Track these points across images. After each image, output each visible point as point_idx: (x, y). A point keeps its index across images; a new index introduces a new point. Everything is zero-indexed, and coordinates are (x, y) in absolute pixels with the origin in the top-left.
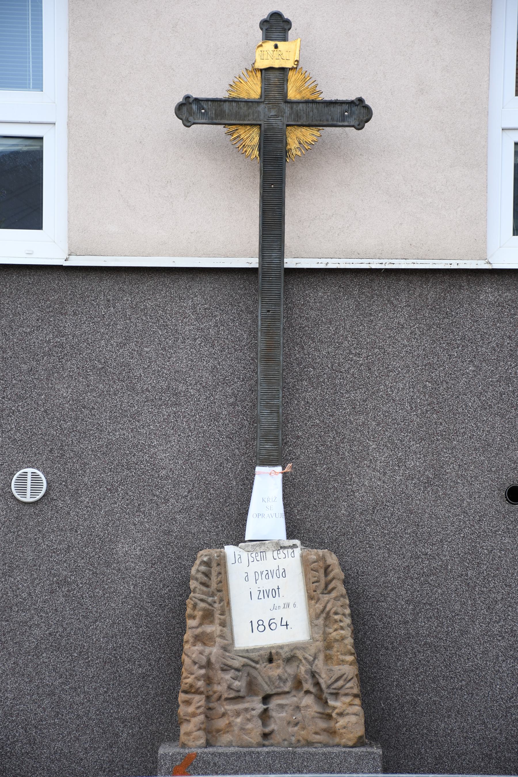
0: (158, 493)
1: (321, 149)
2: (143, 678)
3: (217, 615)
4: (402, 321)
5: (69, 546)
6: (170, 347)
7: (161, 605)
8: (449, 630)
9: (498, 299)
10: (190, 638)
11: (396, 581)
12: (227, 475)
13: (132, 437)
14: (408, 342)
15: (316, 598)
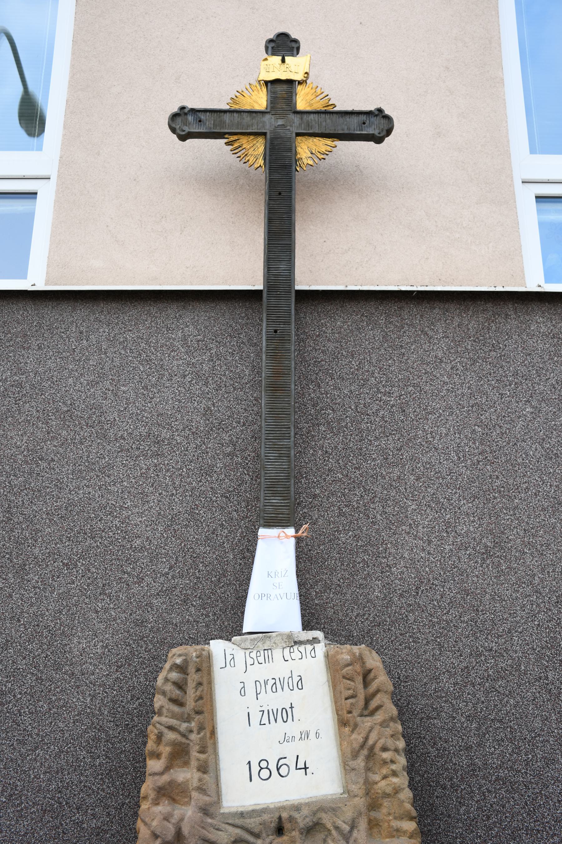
0: (129, 570)
1: (334, 185)
2: (97, 835)
3: (194, 754)
4: (440, 354)
5: (7, 641)
6: (152, 386)
7: (128, 725)
8: (528, 758)
9: (552, 330)
10: (150, 792)
11: (452, 689)
12: (222, 545)
13: (99, 497)
14: (449, 378)
15: (352, 723)
